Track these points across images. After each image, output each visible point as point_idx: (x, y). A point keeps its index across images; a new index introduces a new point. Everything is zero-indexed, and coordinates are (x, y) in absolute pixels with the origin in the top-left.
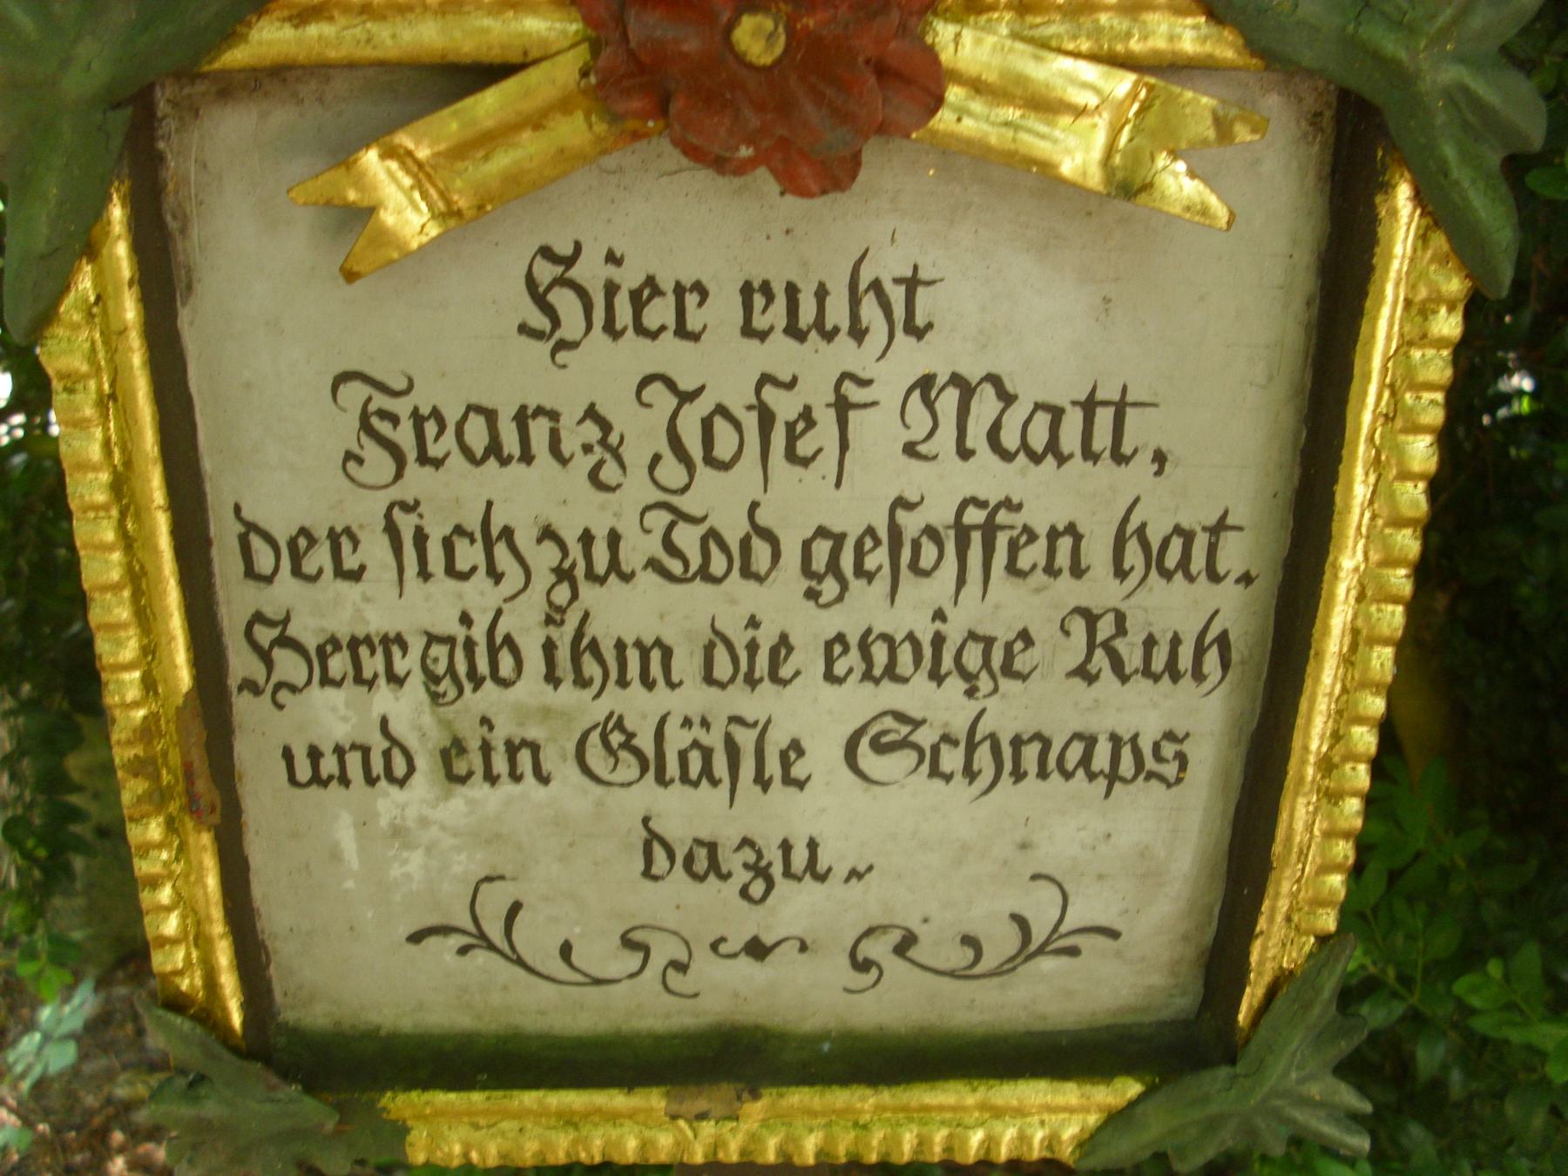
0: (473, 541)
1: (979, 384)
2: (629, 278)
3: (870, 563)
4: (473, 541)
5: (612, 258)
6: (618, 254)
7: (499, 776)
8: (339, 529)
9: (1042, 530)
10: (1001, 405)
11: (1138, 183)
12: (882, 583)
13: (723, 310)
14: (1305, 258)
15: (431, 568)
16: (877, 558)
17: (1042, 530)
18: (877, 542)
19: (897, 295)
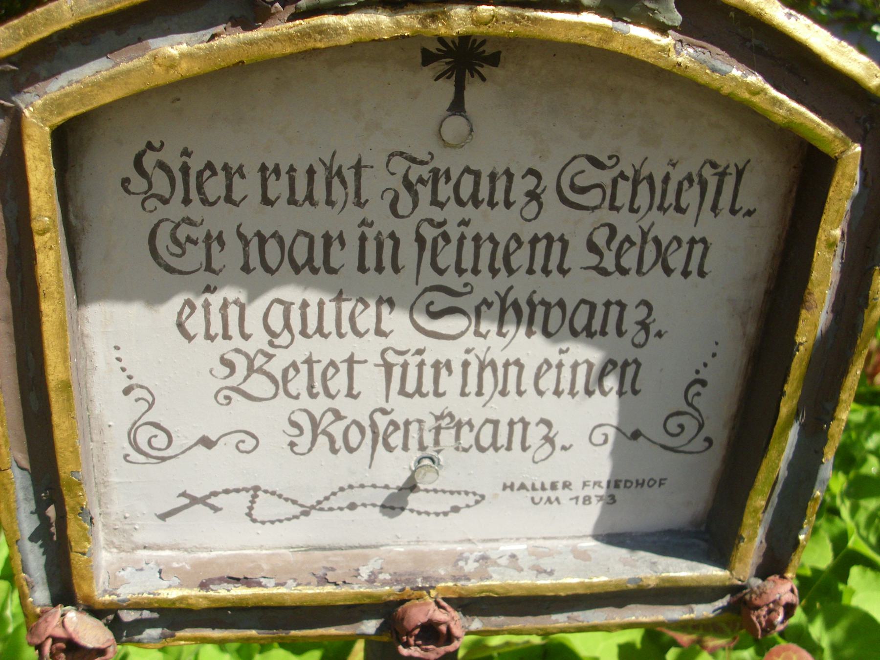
0: (471, 430)
1: (489, 447)
2: (196, 165)
4: (471, 430)
5: (186, 153)
6: (189, 150)
7: (691, 272)
9: (685, 239)
10: (641, 439)
13: (247, 187)
14: (21, 418)
17: (685, 239)
19: (349, 176)
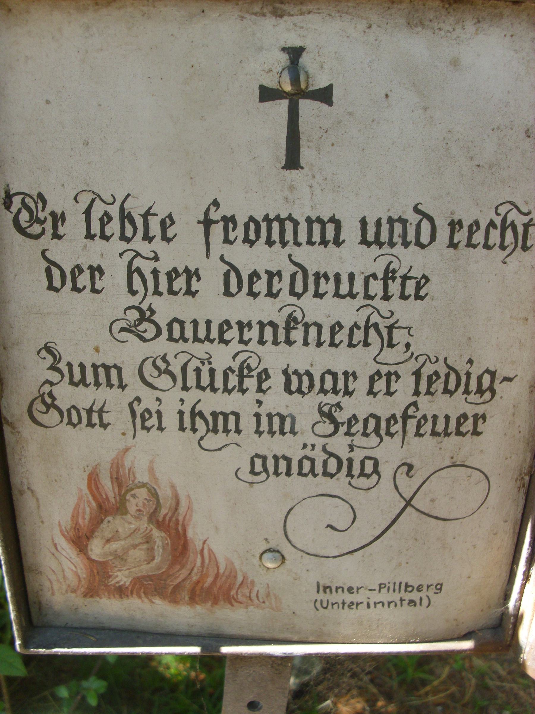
3: (393, 430)
8: (272, 216)
11: (123, 596)
12: (398, 438)
15: (79, 369)
16: (397, 428)
18: (396, 422)
